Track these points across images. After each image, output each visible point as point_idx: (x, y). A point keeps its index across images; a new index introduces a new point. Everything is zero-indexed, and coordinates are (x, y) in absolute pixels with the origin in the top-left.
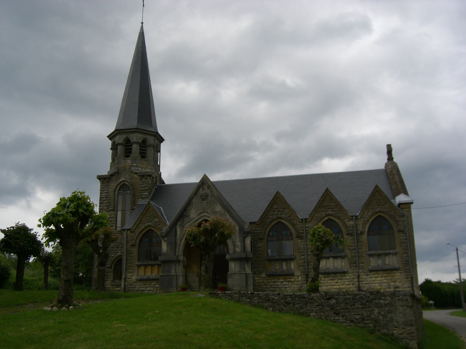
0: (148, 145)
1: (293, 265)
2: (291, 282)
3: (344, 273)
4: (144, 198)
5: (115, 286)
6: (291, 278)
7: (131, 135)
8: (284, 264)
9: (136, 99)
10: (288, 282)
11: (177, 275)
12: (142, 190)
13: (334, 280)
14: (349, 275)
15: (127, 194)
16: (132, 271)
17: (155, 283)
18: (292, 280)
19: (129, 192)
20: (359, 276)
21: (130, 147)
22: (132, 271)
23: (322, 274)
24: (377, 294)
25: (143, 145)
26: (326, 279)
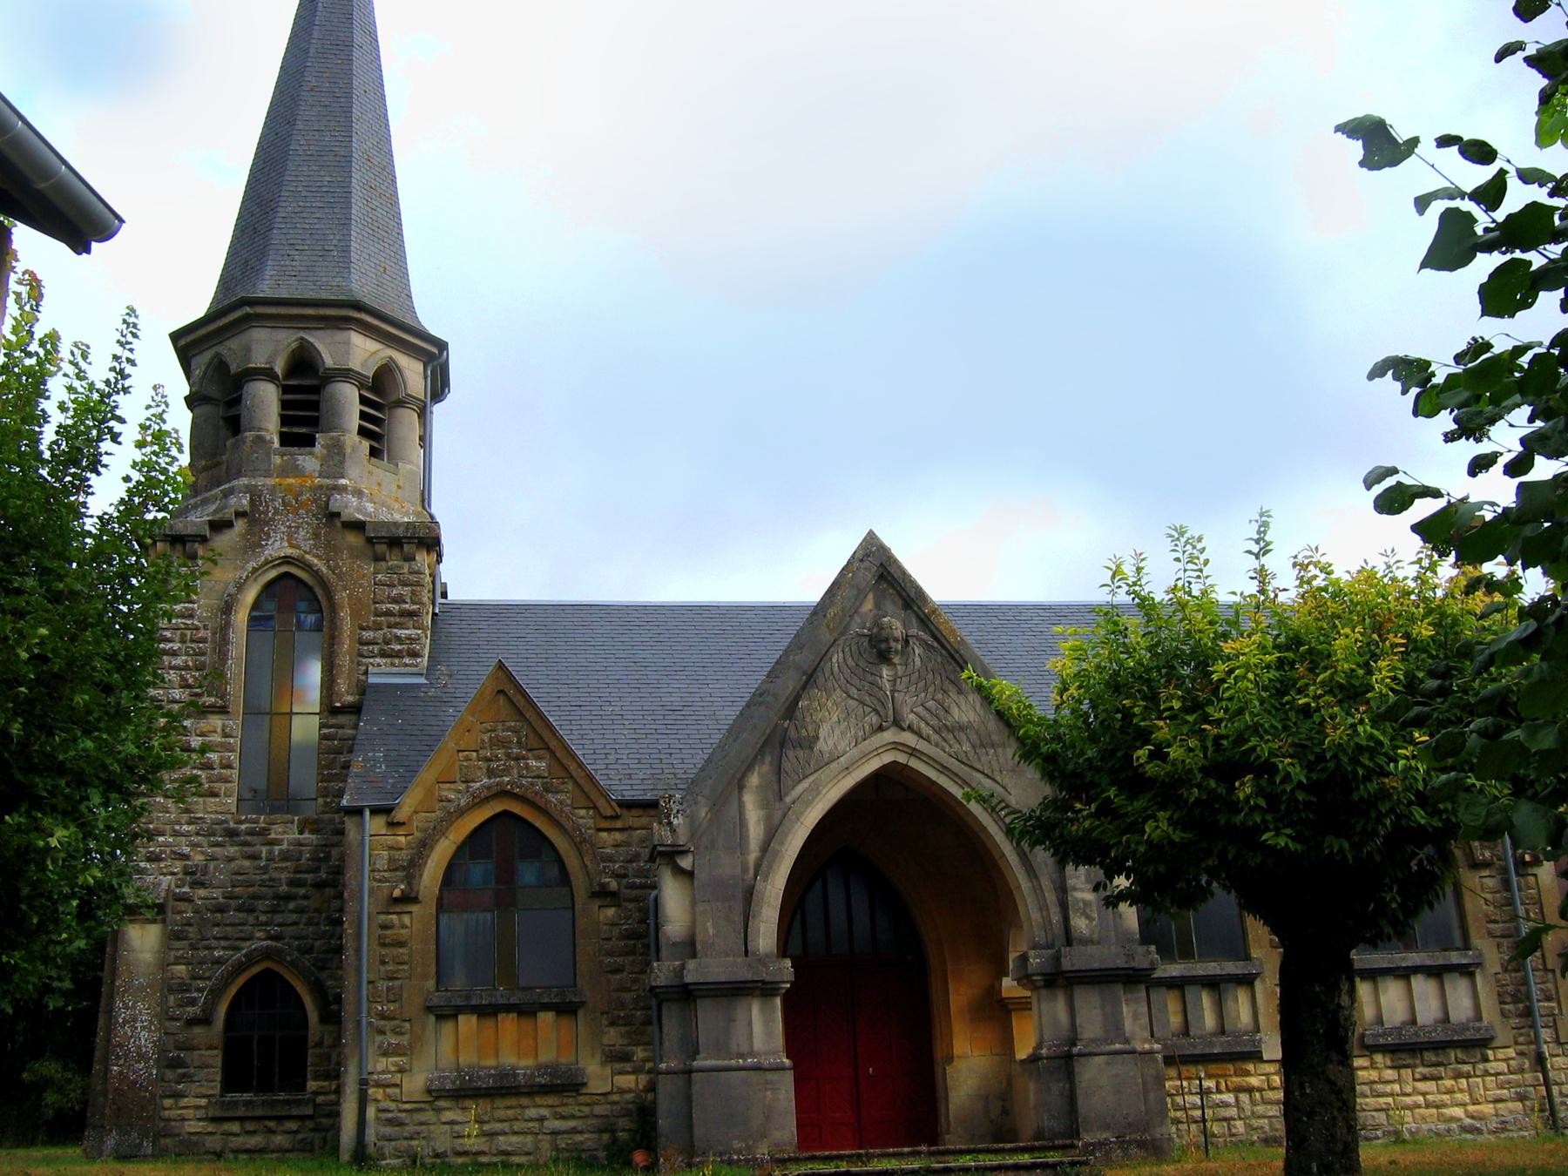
0: (393, 398)
1: (1241, 1008)
2: (1250, 1090)
3: (1476, 1044)
4: (399, 654)
5: (235, 1127)
6: (1248, 1074)
7: (234, 344)
8: (1206, 1000)
9: (40, 197)
10: (1238, 1090)
11: (689, 1072)
12: (388, 613)
13: (1438, 1078)
14: (1501, 1054)
15: (300, 626)
16: (405, 1040)
17: (545, 1112)
18: (1254, 1081)
19: (311, 618)
20: (1540, 1061)
21: (313, 397)
22: (405, 1040)
23: (1371, 1049)
24: (104, 953)
25: (381, 392)
26: (1407, 1073)
